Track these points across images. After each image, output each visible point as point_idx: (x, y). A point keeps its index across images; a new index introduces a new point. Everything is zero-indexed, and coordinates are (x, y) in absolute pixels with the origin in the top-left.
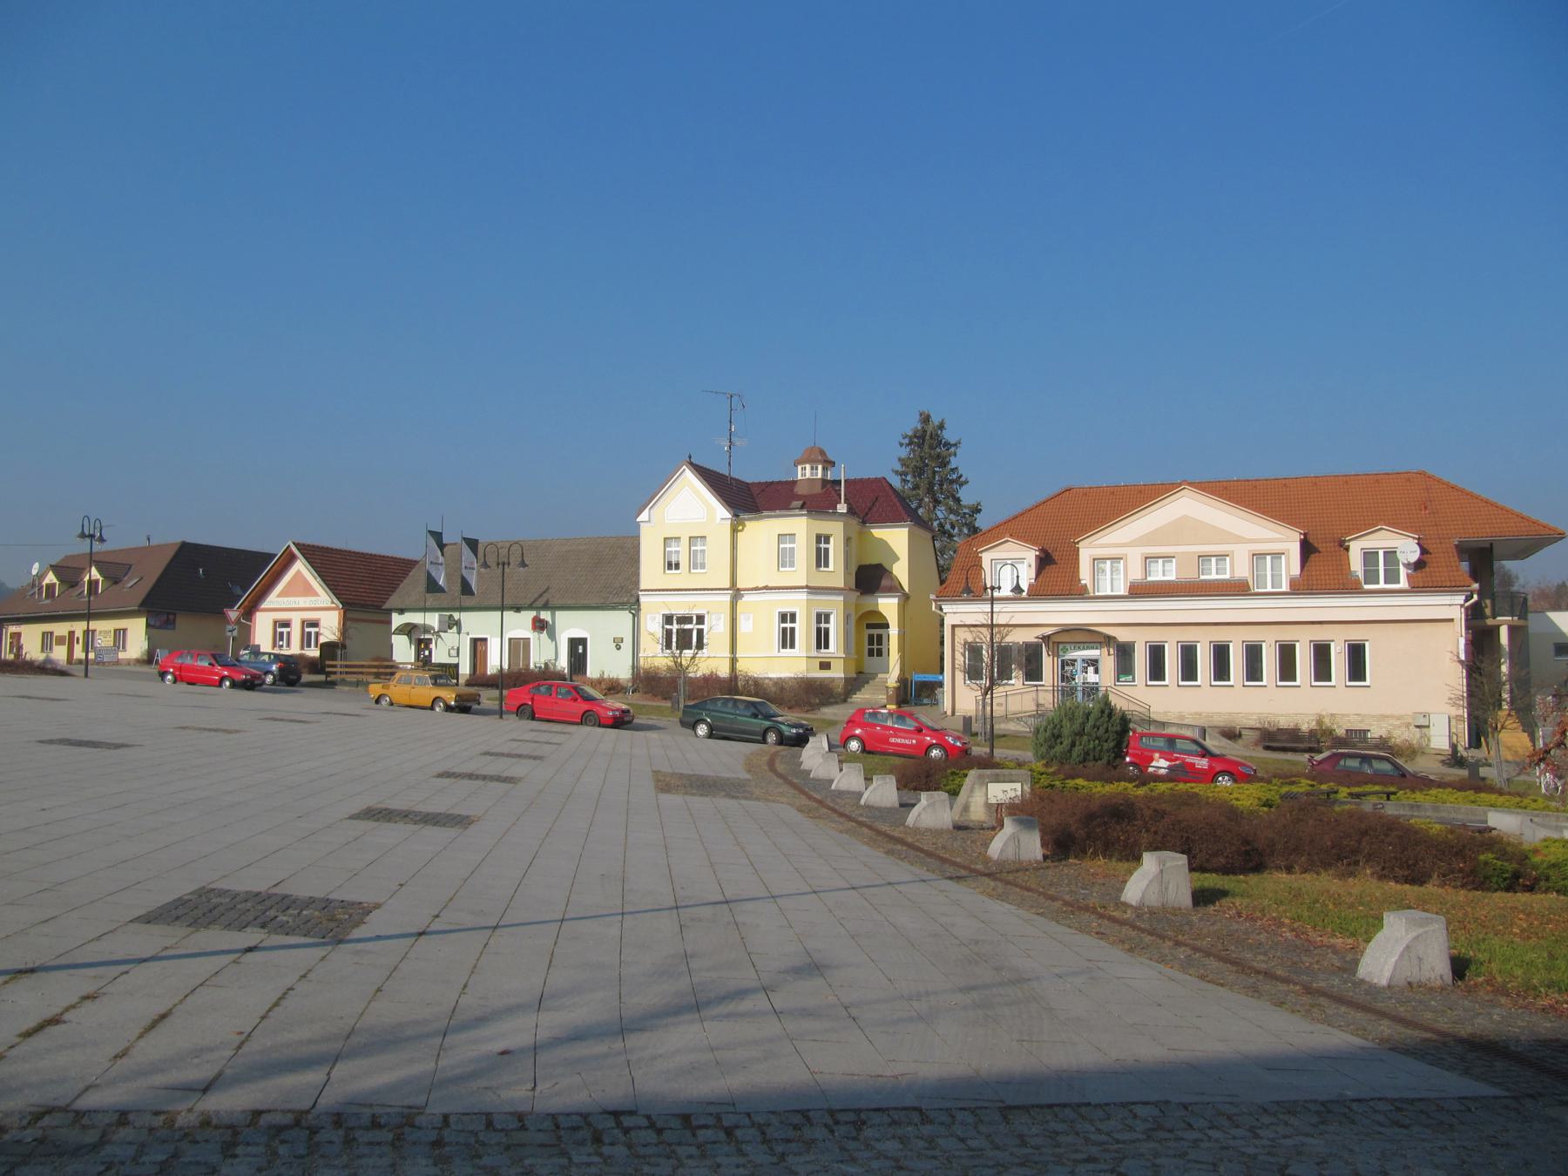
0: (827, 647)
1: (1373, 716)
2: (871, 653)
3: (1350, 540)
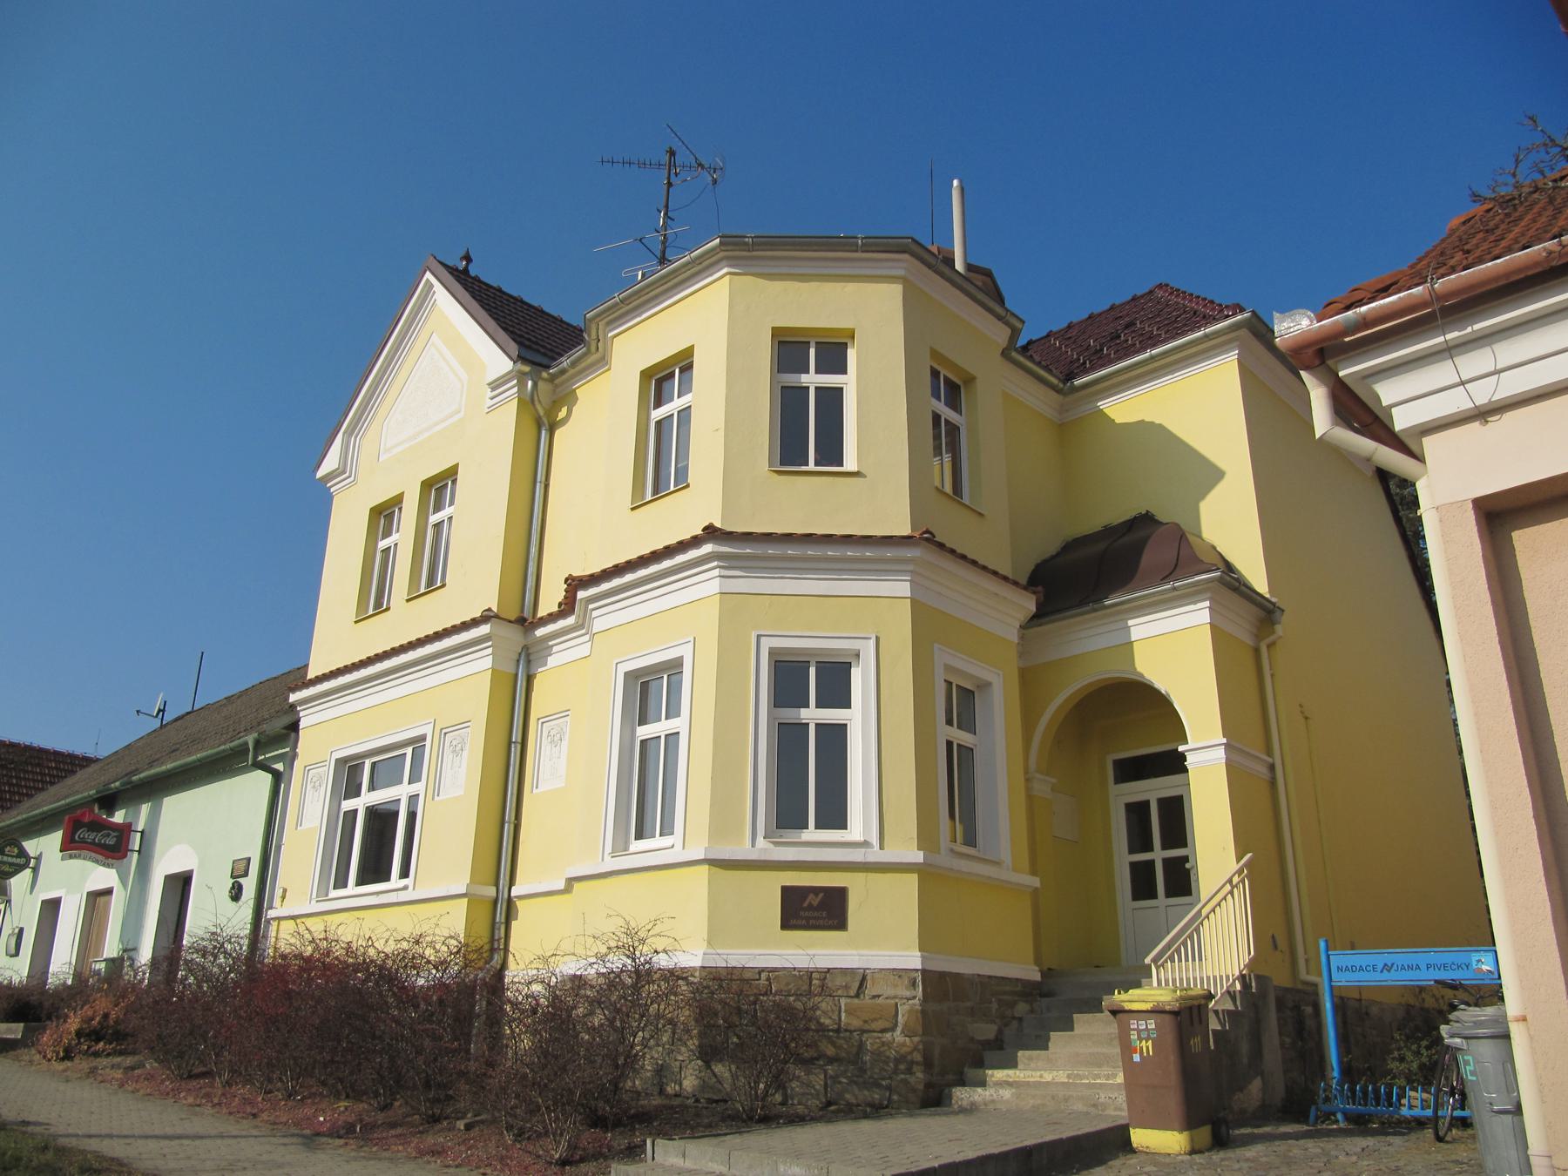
0: (834, 815)
2: (1143, 885)
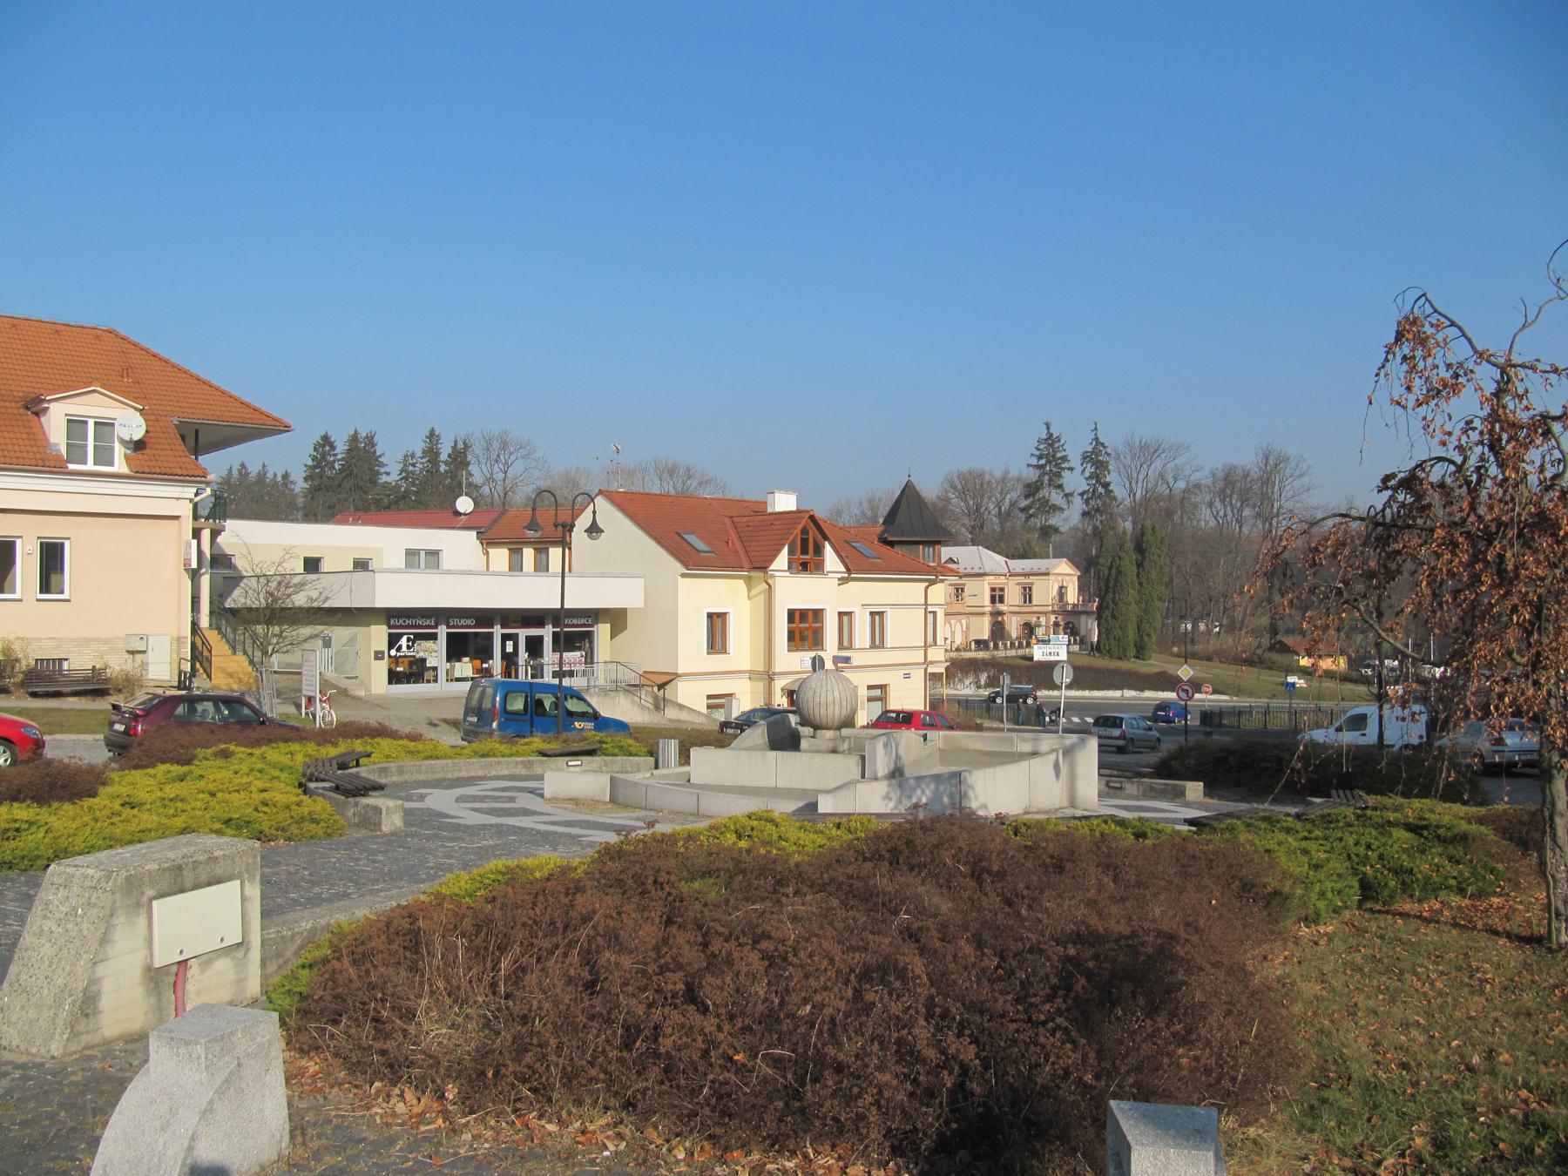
1: (74, 640)
3: (50, 401)
